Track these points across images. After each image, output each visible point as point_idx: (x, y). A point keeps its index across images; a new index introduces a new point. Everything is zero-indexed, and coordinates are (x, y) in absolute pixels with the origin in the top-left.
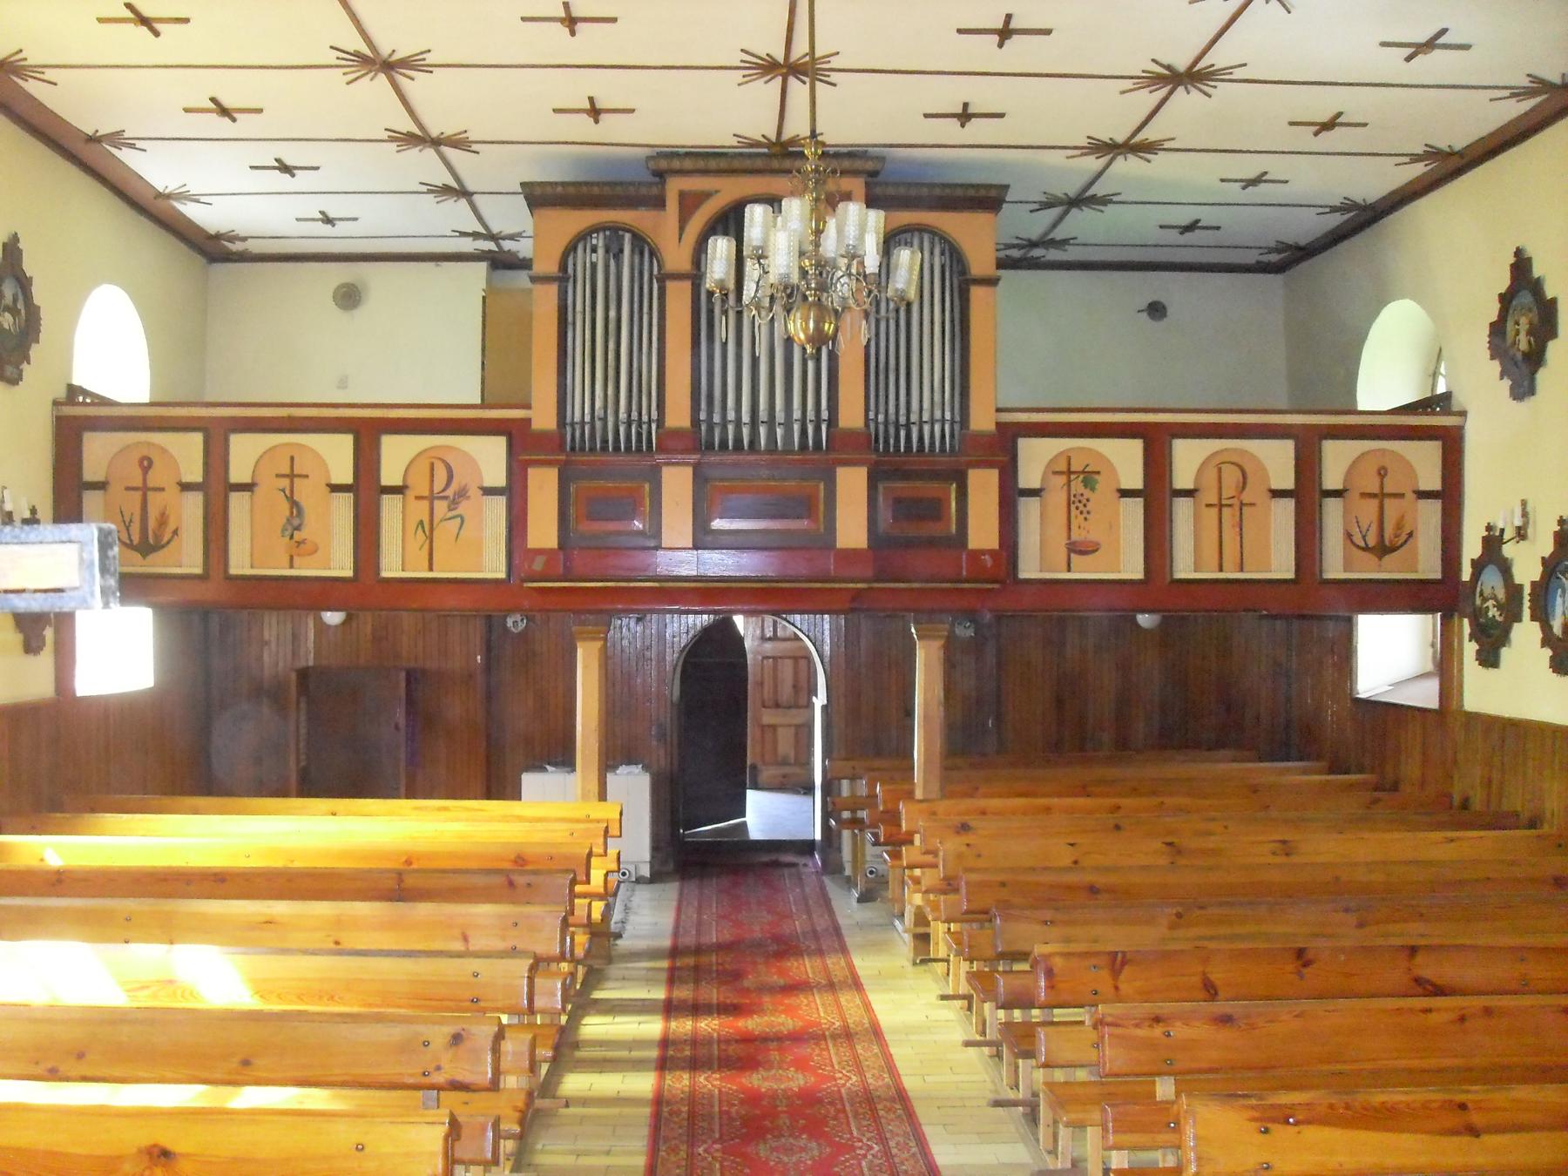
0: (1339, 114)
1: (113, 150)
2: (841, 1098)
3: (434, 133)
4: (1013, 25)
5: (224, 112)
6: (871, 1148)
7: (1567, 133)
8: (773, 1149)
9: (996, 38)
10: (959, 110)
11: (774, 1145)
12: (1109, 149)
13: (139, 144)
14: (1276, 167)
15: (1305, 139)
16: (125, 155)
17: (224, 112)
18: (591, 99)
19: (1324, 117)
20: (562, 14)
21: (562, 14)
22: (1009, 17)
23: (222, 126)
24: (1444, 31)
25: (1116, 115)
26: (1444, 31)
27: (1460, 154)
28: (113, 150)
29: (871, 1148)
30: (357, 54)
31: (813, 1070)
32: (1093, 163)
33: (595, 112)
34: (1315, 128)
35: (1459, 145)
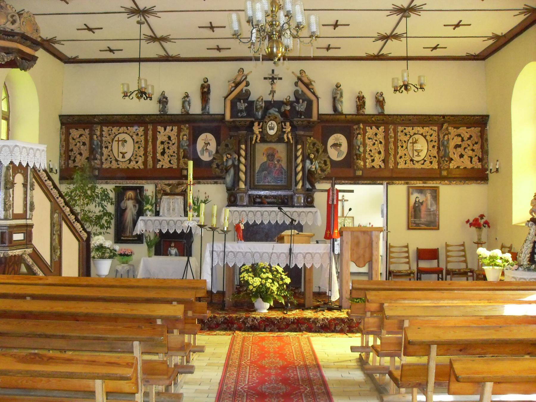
0: (438, 45)
1: (53, 45)
2: (298, 380)
3: (159, 35)
4: (338, 23)
5: (90, 29)
6: (306, 389)
7: (535, 31)
8: (280, 389)
9: (333, 27)
10: (334, 23)
11: (280, 391)
12: (385, 38)
13: (62, 42)
14: (442, 42)
15: (450, 31)
16: (56, 46)
17: (90, 29)
18: (211, 23)
19: (434, 46)
20: (209, 25)
21: (209, 25)
22: (337, 21)
23: (88, 35)
24: (461, 21)
25: (386, 24)
26: (461, 21)
27: (505, 36)
28: (53, 45)
29: (306, 389)
30: (151, 36)
31: (283, 342)
32: (381, 43)
33: (212, 28)
34: (453, 27)
35: (505, 31)
